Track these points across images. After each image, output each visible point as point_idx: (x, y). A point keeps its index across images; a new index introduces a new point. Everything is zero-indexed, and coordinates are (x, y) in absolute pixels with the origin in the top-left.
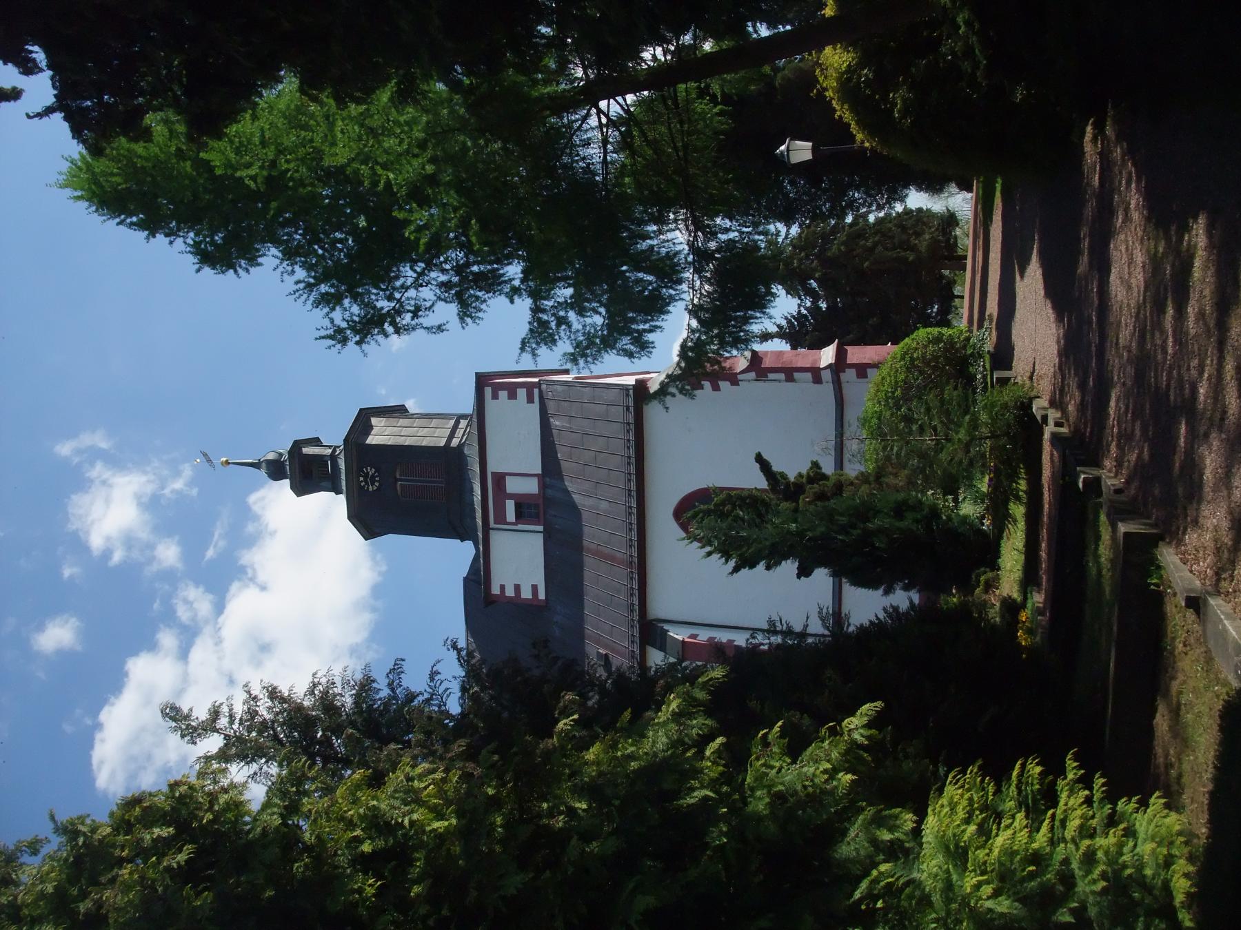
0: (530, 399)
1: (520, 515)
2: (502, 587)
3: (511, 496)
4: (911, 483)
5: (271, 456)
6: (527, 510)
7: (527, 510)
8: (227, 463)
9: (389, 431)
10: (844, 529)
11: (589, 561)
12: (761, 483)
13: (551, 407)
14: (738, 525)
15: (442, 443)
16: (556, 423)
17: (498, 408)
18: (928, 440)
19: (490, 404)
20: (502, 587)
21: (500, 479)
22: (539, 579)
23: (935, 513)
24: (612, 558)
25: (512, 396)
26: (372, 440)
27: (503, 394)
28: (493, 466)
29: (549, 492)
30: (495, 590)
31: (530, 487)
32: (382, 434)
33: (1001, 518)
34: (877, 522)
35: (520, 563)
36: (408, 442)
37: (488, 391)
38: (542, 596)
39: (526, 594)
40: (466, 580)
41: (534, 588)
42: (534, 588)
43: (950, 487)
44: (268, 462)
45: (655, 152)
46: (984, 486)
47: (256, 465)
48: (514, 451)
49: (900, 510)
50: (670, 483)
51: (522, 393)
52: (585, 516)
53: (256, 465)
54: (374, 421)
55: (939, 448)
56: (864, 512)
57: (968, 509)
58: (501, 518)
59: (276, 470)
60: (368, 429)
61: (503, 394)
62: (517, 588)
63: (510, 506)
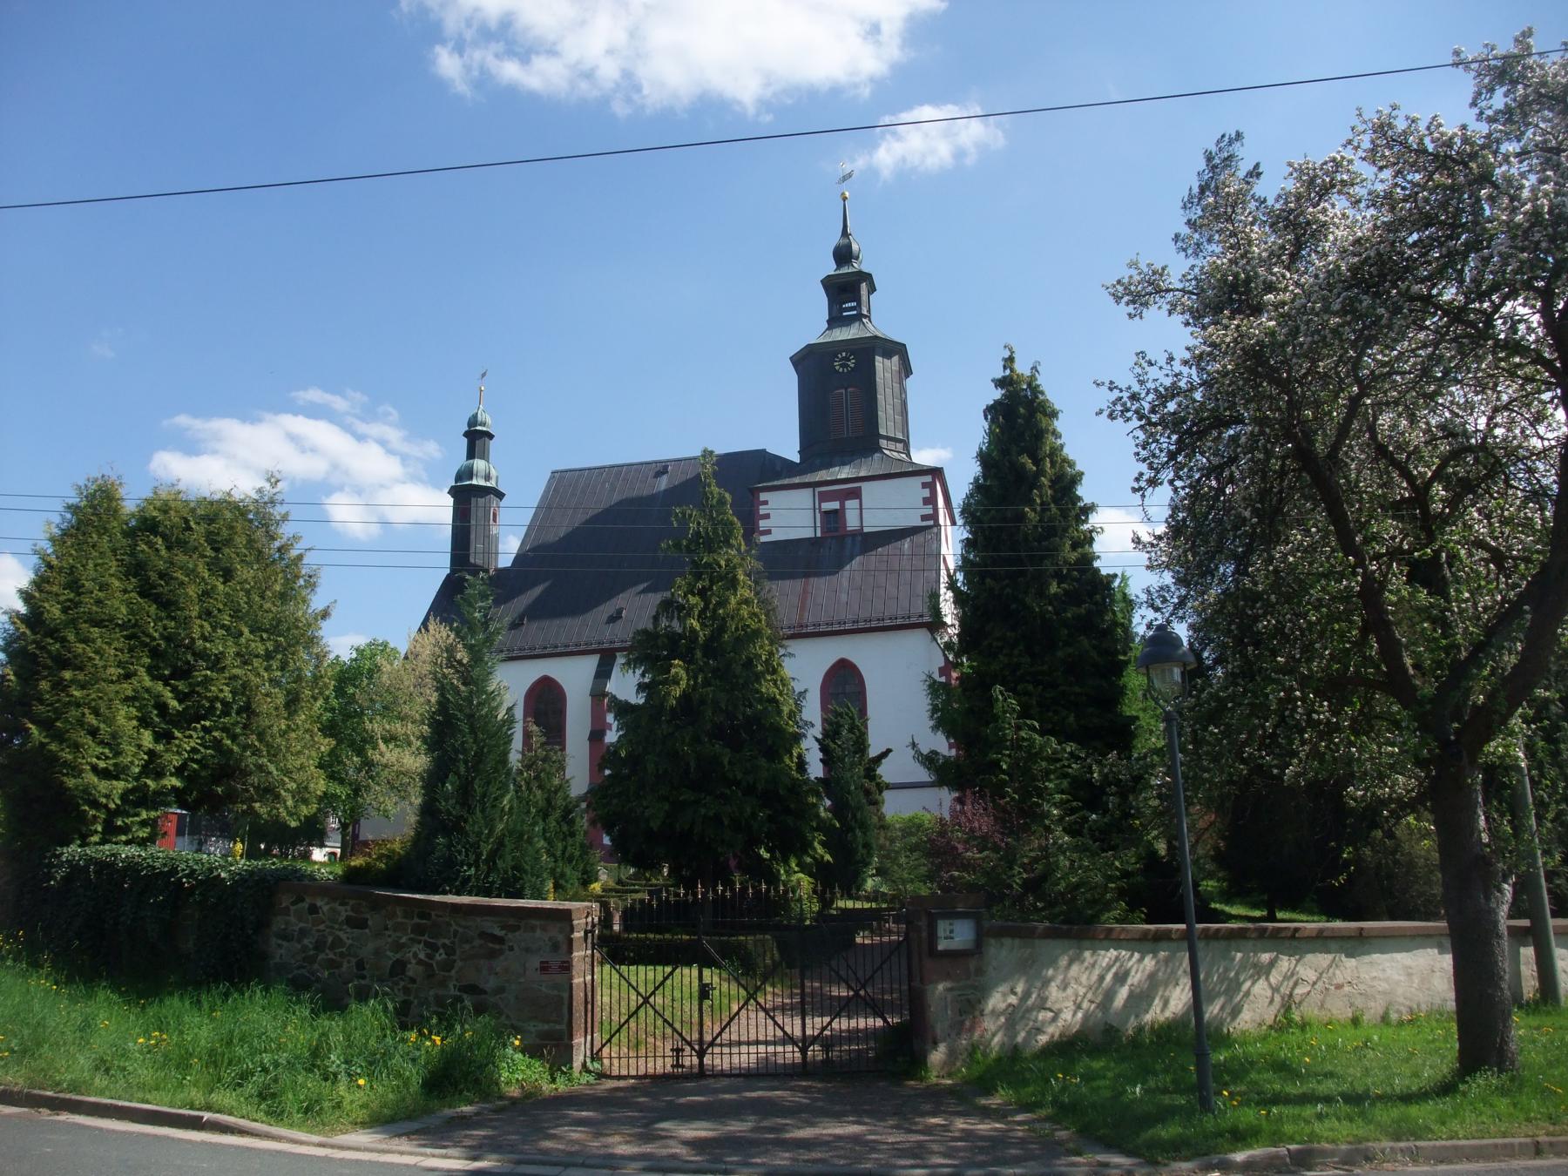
0: (924, 518)
1: (827, 514)
2: (766, 503)
3: (843, 505)
4: (882, 847)
5: (855, 247)
6: (833, 520)
7: (833, 520)
8: (845, 199)
9: (888, 375)
10: (854, 816)
11: (798, 584)
12: (873, 752)
13: (919, 538)
14: (844, 684)
15: (882, 432)
16: (906, 544)
17: (913, 489)
18: (903, 860)
19: (917, 482)
20: (766, 503)
21: (856, 494)
22: (778, 535)
23: (867, 864)
24: (803, 608)
25: (926, 501)
26: (878, 359)
27: (926, 493)
28: (866, 487)
29: (849, 541)
30: (763, 496)
31: (852, 521)
32: (884, 368)
33: (868, 899)
34: (858, 833)
35: (789, 516)
36: (880, 397)
37: (928, 479)
38: (764, 539)
39: (763, 524)
40: (762, 454)
41: (769, 532)
42: (769, 532)
43: (881, 872)
44: (850, 246)
45: (1173, 397)
46: (884, 889)
47: (845, 233)
48: (885, 505)
49: (867, 846)
50: (866, 654)
51: (929, 510)
52: (834, 578)
53: (845, 233)
54: (896, 359)
55: (900, 866)
56: (864, 826)
57: (870, 884)
58: (824, 497)
59: (844, 254)
60: (888, 355)
61: (926, 493)
62: (767, 516)
63: (835, 505)
